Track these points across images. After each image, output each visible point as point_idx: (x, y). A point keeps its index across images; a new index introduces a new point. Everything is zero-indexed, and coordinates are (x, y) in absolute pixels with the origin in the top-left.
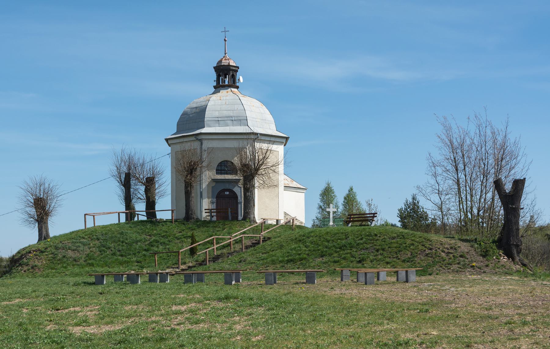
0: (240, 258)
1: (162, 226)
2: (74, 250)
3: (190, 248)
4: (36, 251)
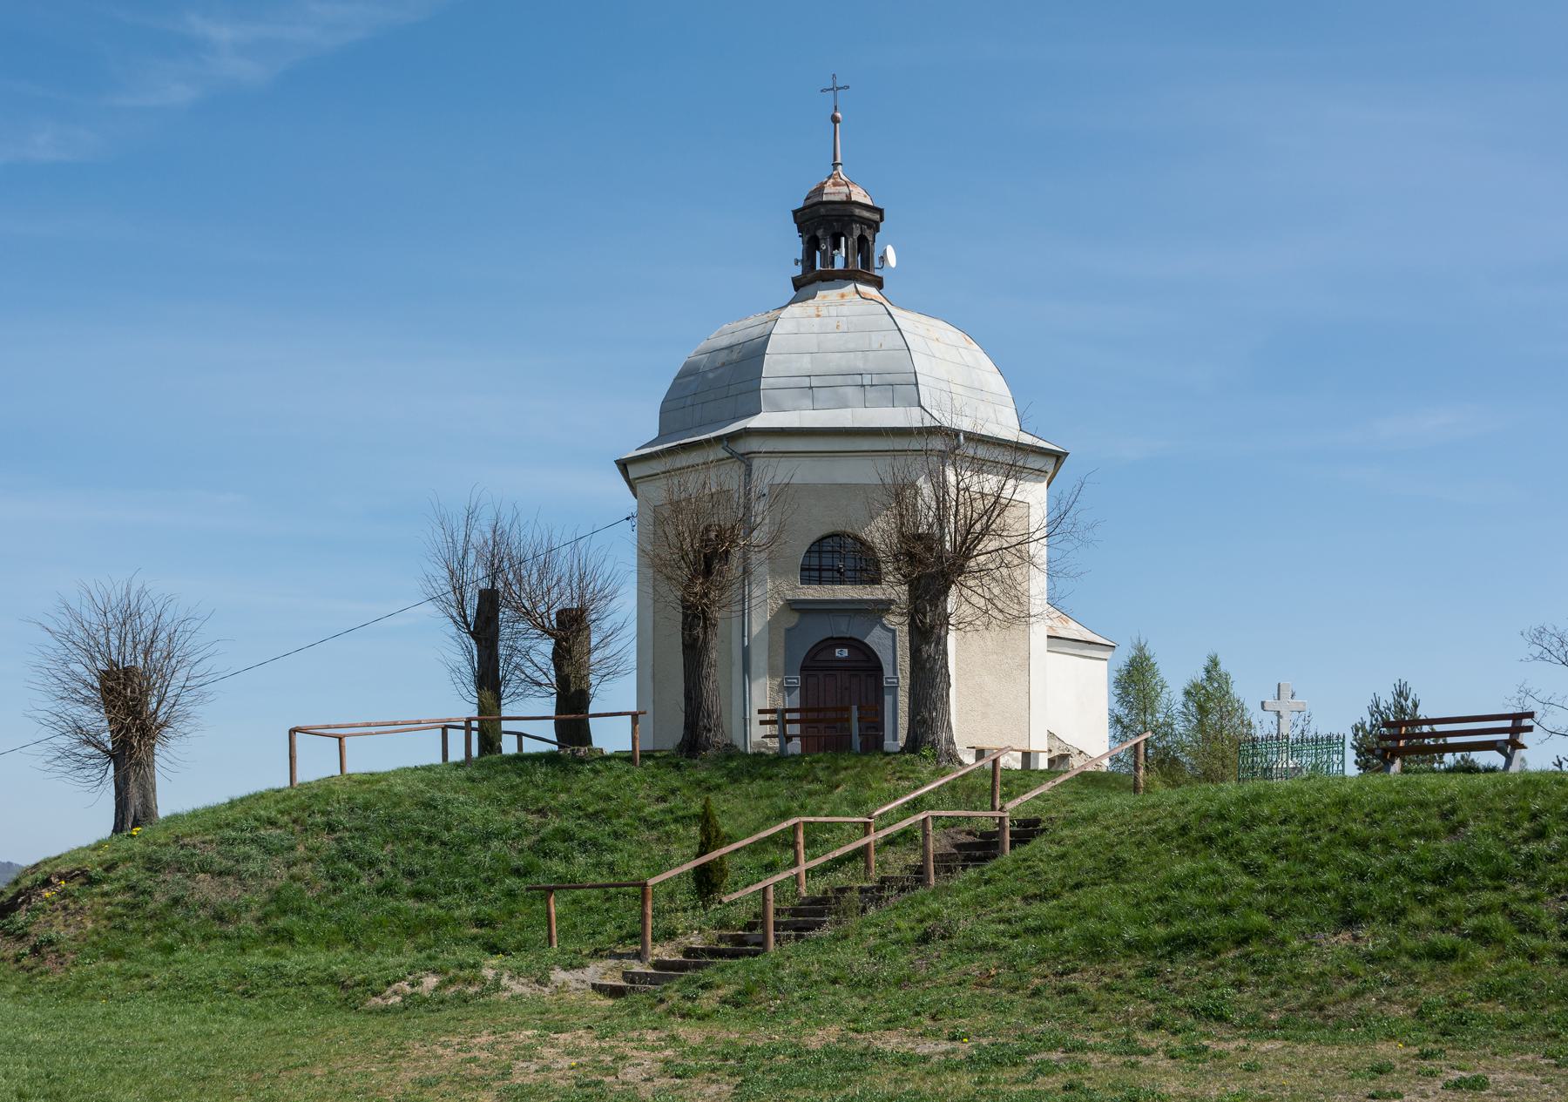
0: (921, 921)
1: (592, 776)
2: (220, 874)
3: (695, 868)
4: (68, 877)
